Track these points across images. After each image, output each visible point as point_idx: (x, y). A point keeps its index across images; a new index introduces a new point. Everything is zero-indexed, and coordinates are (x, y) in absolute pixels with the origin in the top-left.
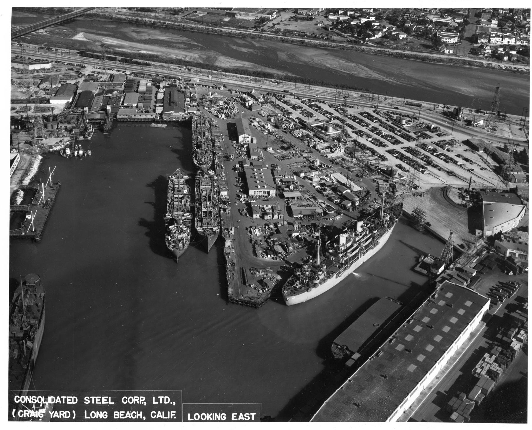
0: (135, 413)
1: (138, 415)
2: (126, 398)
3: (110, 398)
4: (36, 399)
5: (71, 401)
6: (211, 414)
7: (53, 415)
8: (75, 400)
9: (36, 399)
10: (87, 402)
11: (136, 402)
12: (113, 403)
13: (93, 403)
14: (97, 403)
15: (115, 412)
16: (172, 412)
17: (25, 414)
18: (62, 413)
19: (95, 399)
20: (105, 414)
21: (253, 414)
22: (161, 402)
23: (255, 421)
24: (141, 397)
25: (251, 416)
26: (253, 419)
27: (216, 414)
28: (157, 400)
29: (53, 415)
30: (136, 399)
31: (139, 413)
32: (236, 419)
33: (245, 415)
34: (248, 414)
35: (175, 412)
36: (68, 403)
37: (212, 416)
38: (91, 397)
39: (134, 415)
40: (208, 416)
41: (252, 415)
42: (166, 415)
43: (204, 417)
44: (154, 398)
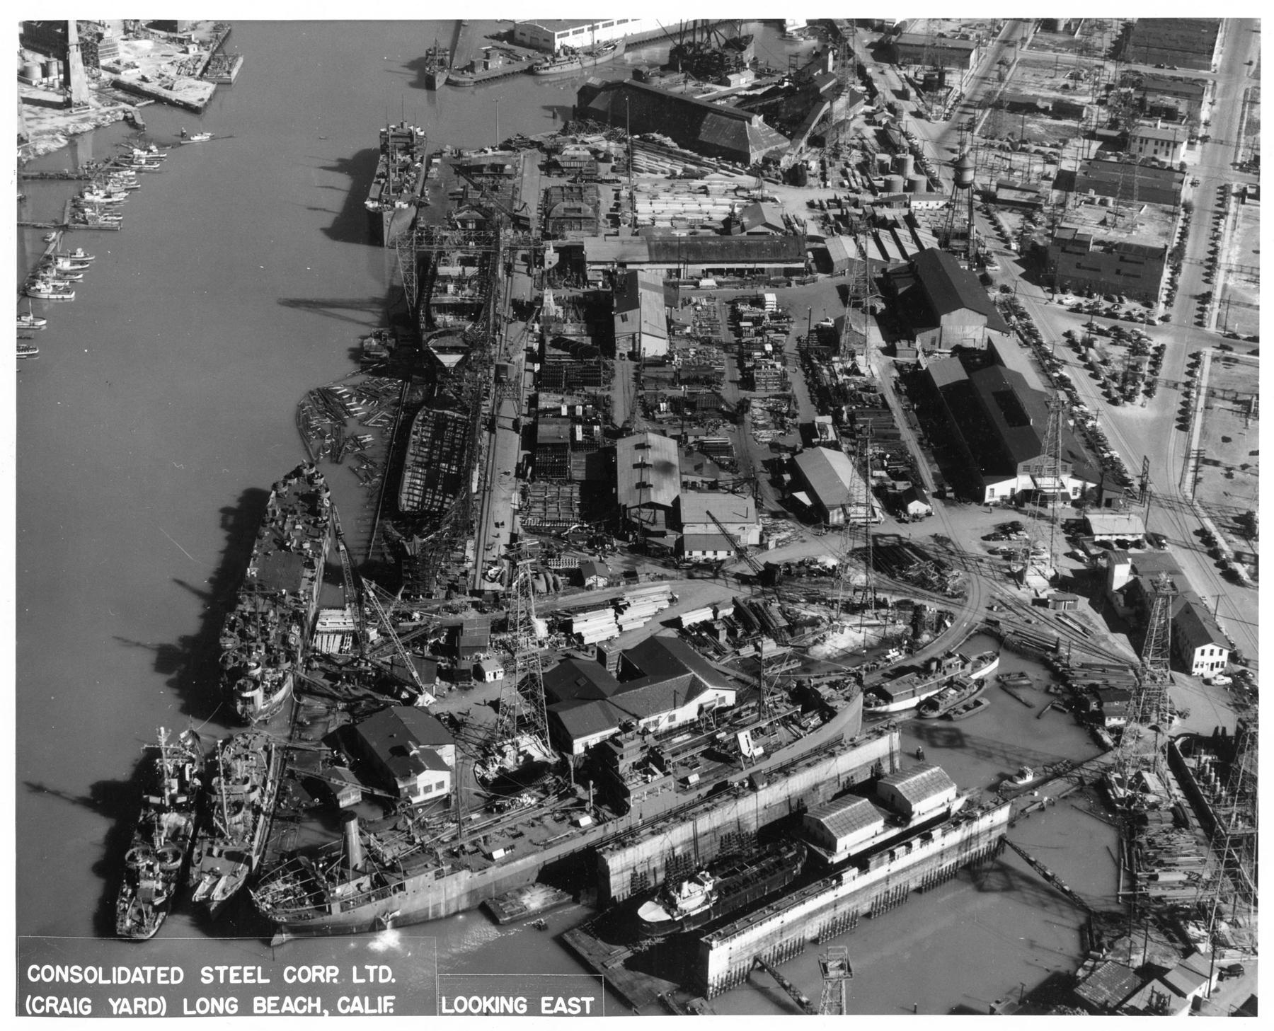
0: (304, 1000)
1: (311, 1005)
2: (294, 969)
3: (259, 969)
4: (82, 972)
5: (168, 978)
6: (492, 999)
7: (119, 1007)
8: (177, 975)
9: (82, 972)
10: (207, 978)
11: (317, 978)
12: (268, 981)
13: (222, 981)
14: (160, 982)
15: (256, 999)
16: (386, 998)
17: (48, 1005)
18: (140, 1003)
19: (227, 973)
20: (521, 1002)
21: (588, 1000)
22: (372, 980)
23: (593, 1014)
24: (329, 968)
25: (583, 1004)
26: (588, 1011)
27: (503, 998)
28: (363, 974)
29: (119, 1007)
30: (318, 971)
31: (314, 1001)
32: (277, 1011)
33: (570, 1002)
34: (577, 1000)
35: (393, 998)
36: (232, 981)
37: (493, 1004)
38: (217, 968)
39: (301, 1005)
40: (486, 1003)
41: (218, 972)
42: (373, 1005)
43: (475, 1004)
44: (355, 969)
